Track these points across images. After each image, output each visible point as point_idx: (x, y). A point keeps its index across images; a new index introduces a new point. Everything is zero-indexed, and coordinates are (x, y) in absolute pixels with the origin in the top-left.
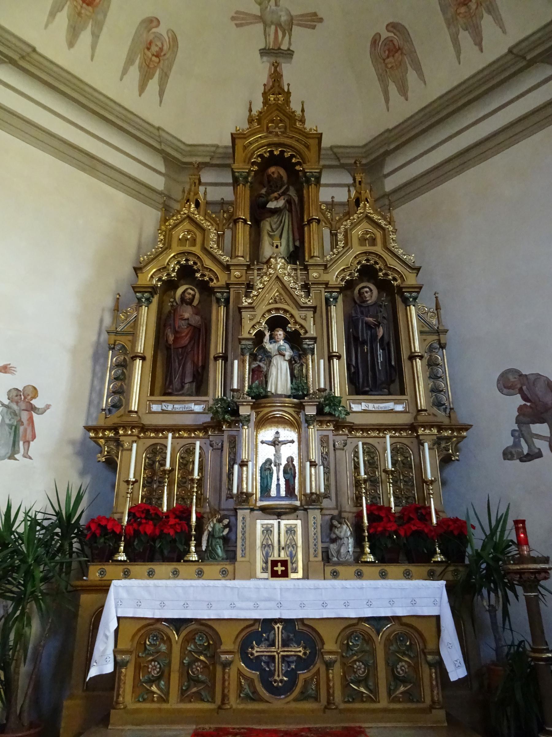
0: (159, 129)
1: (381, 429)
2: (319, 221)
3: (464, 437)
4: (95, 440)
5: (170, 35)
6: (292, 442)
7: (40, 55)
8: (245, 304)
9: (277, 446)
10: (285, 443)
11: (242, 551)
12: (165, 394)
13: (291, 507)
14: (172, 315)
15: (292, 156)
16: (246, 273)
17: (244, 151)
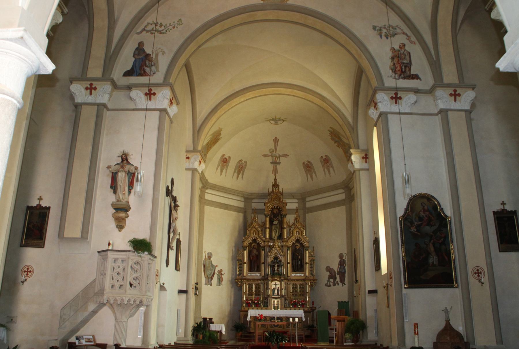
1: (298, 280)
6: (279, 284)
10: (277, 284)
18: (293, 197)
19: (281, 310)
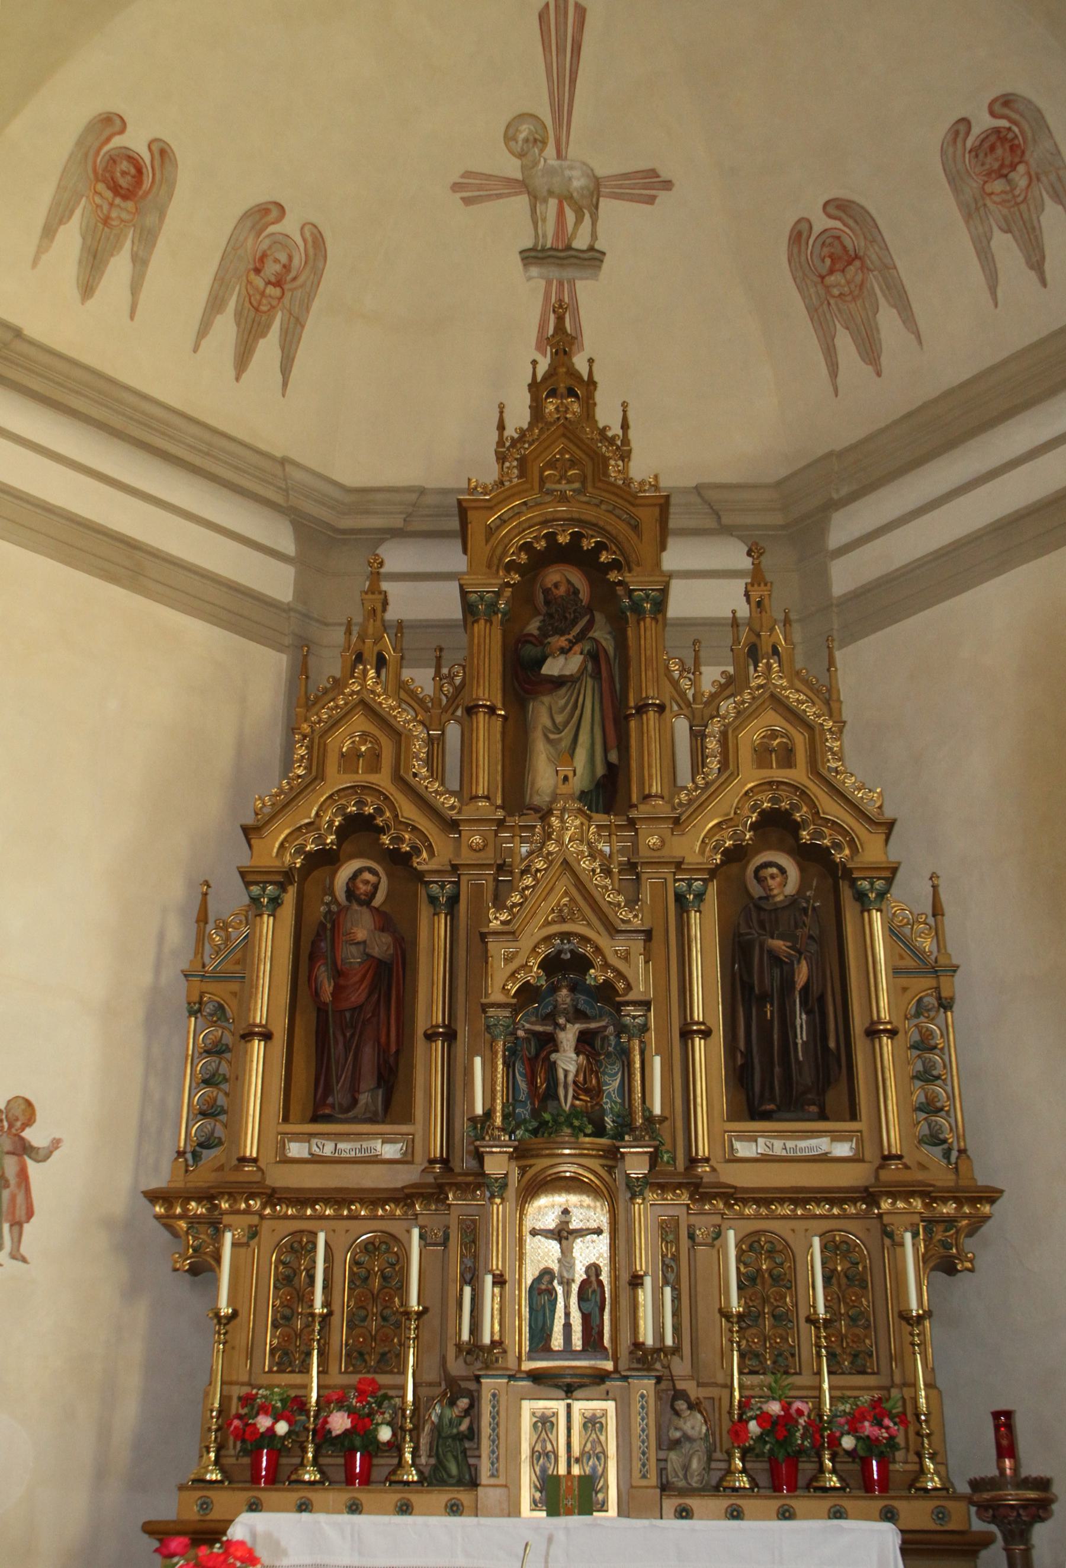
0: (284, 461)
2: (661, 708)
3: (987, 1218)
4: (166, 1221)
5: (308, 235)
6: (598, 1232)
7: (32, 343)
8: (495, 924)
9: (564, 1242)
10: (581, 1233)
11: (492, 1464)
12: (315, 1119)
13: (589, 1371)
14: (328, 933)
15: (600, 547)
16: (496, 835)
17: (487, 541)
18: (710, 523)
19: (625, 1521)
